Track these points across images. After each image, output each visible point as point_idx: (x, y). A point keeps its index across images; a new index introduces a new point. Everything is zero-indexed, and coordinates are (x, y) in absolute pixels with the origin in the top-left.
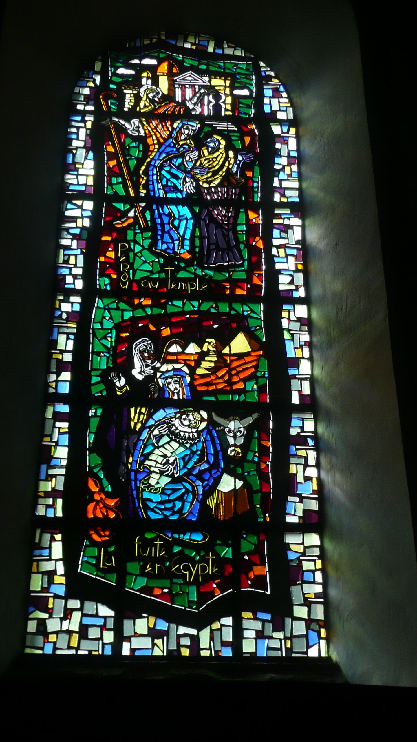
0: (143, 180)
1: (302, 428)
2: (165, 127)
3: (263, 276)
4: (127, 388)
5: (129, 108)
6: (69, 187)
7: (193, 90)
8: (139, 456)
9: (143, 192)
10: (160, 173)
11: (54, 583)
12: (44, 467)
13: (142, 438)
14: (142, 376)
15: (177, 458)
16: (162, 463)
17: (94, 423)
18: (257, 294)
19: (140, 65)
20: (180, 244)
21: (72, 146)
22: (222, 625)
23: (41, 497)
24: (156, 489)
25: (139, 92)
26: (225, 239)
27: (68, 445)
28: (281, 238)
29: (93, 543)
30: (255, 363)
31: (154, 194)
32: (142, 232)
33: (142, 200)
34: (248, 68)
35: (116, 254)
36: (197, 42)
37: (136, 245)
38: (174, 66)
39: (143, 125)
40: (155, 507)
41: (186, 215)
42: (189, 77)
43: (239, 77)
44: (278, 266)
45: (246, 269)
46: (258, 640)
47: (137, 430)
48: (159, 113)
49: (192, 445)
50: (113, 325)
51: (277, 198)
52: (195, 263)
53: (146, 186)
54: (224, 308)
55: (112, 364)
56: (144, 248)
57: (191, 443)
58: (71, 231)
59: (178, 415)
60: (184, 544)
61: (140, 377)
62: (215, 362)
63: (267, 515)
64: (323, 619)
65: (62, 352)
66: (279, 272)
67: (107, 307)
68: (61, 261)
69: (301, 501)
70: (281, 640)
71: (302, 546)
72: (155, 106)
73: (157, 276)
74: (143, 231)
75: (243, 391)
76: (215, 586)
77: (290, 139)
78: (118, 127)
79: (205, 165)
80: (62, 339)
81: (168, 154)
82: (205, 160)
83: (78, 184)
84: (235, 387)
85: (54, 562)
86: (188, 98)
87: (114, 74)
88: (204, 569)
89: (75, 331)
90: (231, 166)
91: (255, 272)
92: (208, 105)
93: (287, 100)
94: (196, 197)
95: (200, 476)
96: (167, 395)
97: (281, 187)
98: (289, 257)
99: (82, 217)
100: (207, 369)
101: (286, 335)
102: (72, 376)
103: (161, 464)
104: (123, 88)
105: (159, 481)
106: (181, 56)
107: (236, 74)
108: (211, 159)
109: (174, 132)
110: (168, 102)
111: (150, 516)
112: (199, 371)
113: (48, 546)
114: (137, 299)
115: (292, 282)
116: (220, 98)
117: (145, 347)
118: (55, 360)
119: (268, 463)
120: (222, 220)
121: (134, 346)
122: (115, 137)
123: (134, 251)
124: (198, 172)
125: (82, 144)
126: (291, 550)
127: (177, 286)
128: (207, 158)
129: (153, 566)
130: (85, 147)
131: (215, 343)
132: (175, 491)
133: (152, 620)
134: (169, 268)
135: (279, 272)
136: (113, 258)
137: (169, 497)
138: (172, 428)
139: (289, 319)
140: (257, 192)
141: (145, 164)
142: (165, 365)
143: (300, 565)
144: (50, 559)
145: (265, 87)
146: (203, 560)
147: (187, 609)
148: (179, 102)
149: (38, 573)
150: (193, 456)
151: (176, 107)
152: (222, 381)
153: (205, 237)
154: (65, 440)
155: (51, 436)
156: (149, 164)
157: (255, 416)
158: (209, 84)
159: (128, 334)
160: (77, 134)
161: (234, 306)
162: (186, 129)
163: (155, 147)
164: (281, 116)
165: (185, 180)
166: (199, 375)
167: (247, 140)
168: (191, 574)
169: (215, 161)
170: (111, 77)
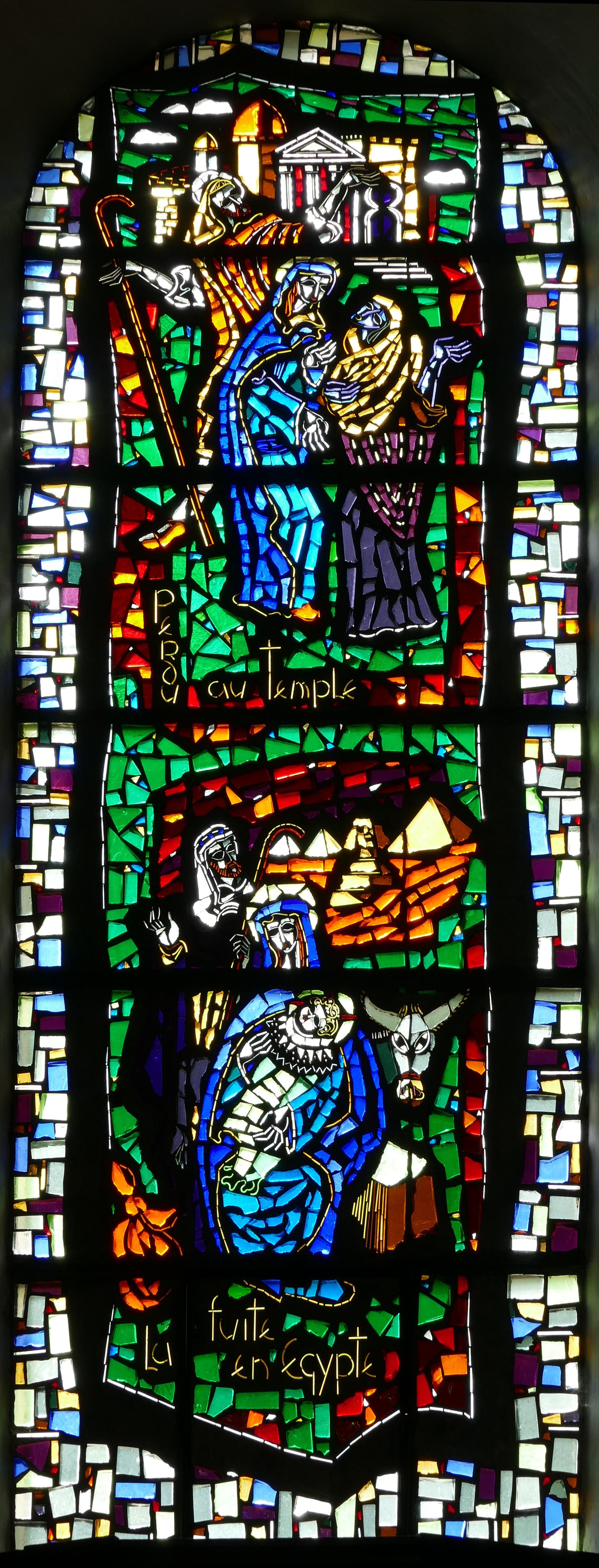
0: (204, 424)
1: (555, 1027)
2: (254, 282)
3: (485, 655)
4: (184, 949)
5: (165, 237)
6: (32, 452)
7: (322, 180)
8: (214, 1110)
9: (205, 456)
10: (246, 405)
11: (58, 1409)
12: (22, 1143)
13: (218, 1066)
14: (214, 916)
15: (292, 1110)
16: (261, 1124)
17: (118, 1034)
18: (469, 702)
19: (189, 118)
20: (294, 586)
21: (32, 343)
22: (379, 1493)
23: (21, 1213)
24: (249, 1185)
25: (189, 192)
26: (398, 567)
27: (67, 1089)
28: (530, 556)
29: (130, 1316)
30: (459, 875)
31: (233, 459)
32: (205, 560)
33: (204, 475)
34: (465, 108)
35: (148, 618)
36: (334, 48)
37: (194, 593)
38: (274, 115)
39: (201, 280)
40: (247, 1226)
41: (306, 509)
42: (314, 144)
43: (441, 137)
44: (520, 630)
45: (445, 640)
46: (448, 1523)
47: (208, 1047)
48: (238, 246)
49: (321, 1078)
50: (148, 794)
51: (524, 453)
52: (328, 633)
53: (212, 441)
54: (392, 741)
55: (150, 892)
56: (211, 601)
57: (319, 1074)
58: (46, 565)
59: (293, 1008)
60: (307, 1311)
61: (210, 921)
62: (372, 877)
63: (474, 1236)
64: (576, 1472)
65: (43, 867)
66: (521, 644)
67: (133, 752)
68: (26, 642)
69: (545, 1202)
70: (491, 1521)
71: (543, 1307)
72: (229, 227)
73: (240, 668)
74: (208, 554)
75: (431, 944)
76: (366, 1403)
77: (563, 295)
78: (138, 285)
79: (352, 377)
80: (40, 833)
81: (263, 353)
82: (353, 363)
83: (54, 445)
84: (415, 935)
85: (55, 1360)
86: (310, 201)
87: (127, 146)
88: (345, 1365)
89: (65, 814)
90: (414, 377)
91: (465, 648)
92: (361, 218)
93: (561, 192)
94: (331, 462)
95: (337, 1152)
96: (268, 963)
97: (535, 426)
98: (547, 604)
99: (68, 528)
100: (354, 894)
101: (532, 803)
102: (66, 925)
103: (258, 1125)
104: (150, 183)
105: (255, 1166)
106: (293, 87)
107: (435, 127)
108: (366, 361)
109: (279, 295)
110: (261, 214)
111: (237, 1248)
112: (339, 900)
113: (41, 1326)
114: (199, 728)
115: (550, 668)
116: (392, 194)
117: (218, 847)
118: (29, 888)
119: (479, 1113)
120: (390, 517)
121: (196, 845)
122: (134, 316)
123: (188, 607)
124: (337, 395)
125: (56, 338)
126: (518, 1315)
127: (287, 693)
128: (357, 356)
129: (246, 1363)
130: (63, 346)
131: (373, 828)
132: (287, 1187)
133: (246, 1483)
134: (269, 647)
135: (521, 644)
136: (142, 627)
137: (275, 1203)
138: (279, 1039)
139: (540, 763)
140: (478, 440)
141: (209, 382)
142: (264, 888)
143: (536, 1350)
144: (47, 1356)
145: (507, 158)
146: (344, 1344)
147: (312, 1457)
148: (287, 210)
149: (26, 1386)
150: (323, 1105)
151: (280, 227)
152: (384, 920)
153: (351, 566)
154: (60, 1077)
155: (31, 1070)
156: (218, 380)
157: (455, 1003)
158: (363, 159)
159: (180, 817)
160: (45, 312)
161: (417, 735)
162: (308, 283)
163: (230, 335)
164: (544, 235)
165: (303, 416)
166: (337, 909)
167: (457, 303)
168: (319, 1376)
169: (378, 363)
170: (120, 156)
